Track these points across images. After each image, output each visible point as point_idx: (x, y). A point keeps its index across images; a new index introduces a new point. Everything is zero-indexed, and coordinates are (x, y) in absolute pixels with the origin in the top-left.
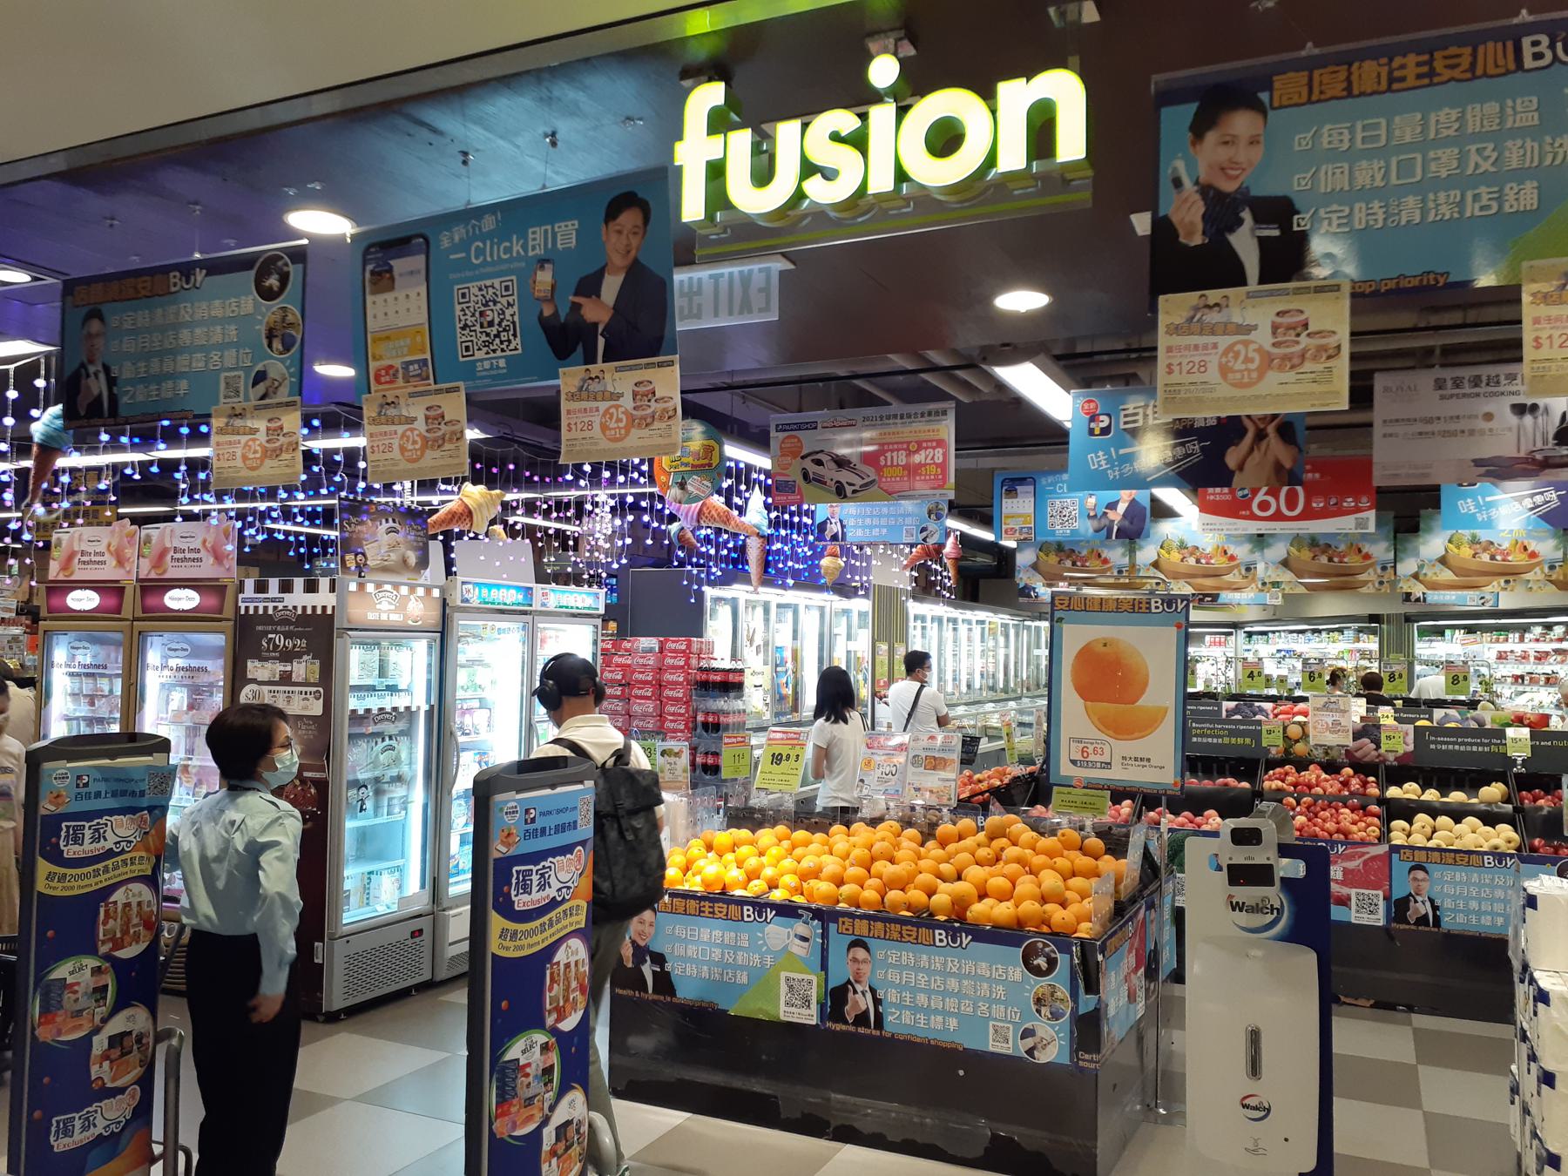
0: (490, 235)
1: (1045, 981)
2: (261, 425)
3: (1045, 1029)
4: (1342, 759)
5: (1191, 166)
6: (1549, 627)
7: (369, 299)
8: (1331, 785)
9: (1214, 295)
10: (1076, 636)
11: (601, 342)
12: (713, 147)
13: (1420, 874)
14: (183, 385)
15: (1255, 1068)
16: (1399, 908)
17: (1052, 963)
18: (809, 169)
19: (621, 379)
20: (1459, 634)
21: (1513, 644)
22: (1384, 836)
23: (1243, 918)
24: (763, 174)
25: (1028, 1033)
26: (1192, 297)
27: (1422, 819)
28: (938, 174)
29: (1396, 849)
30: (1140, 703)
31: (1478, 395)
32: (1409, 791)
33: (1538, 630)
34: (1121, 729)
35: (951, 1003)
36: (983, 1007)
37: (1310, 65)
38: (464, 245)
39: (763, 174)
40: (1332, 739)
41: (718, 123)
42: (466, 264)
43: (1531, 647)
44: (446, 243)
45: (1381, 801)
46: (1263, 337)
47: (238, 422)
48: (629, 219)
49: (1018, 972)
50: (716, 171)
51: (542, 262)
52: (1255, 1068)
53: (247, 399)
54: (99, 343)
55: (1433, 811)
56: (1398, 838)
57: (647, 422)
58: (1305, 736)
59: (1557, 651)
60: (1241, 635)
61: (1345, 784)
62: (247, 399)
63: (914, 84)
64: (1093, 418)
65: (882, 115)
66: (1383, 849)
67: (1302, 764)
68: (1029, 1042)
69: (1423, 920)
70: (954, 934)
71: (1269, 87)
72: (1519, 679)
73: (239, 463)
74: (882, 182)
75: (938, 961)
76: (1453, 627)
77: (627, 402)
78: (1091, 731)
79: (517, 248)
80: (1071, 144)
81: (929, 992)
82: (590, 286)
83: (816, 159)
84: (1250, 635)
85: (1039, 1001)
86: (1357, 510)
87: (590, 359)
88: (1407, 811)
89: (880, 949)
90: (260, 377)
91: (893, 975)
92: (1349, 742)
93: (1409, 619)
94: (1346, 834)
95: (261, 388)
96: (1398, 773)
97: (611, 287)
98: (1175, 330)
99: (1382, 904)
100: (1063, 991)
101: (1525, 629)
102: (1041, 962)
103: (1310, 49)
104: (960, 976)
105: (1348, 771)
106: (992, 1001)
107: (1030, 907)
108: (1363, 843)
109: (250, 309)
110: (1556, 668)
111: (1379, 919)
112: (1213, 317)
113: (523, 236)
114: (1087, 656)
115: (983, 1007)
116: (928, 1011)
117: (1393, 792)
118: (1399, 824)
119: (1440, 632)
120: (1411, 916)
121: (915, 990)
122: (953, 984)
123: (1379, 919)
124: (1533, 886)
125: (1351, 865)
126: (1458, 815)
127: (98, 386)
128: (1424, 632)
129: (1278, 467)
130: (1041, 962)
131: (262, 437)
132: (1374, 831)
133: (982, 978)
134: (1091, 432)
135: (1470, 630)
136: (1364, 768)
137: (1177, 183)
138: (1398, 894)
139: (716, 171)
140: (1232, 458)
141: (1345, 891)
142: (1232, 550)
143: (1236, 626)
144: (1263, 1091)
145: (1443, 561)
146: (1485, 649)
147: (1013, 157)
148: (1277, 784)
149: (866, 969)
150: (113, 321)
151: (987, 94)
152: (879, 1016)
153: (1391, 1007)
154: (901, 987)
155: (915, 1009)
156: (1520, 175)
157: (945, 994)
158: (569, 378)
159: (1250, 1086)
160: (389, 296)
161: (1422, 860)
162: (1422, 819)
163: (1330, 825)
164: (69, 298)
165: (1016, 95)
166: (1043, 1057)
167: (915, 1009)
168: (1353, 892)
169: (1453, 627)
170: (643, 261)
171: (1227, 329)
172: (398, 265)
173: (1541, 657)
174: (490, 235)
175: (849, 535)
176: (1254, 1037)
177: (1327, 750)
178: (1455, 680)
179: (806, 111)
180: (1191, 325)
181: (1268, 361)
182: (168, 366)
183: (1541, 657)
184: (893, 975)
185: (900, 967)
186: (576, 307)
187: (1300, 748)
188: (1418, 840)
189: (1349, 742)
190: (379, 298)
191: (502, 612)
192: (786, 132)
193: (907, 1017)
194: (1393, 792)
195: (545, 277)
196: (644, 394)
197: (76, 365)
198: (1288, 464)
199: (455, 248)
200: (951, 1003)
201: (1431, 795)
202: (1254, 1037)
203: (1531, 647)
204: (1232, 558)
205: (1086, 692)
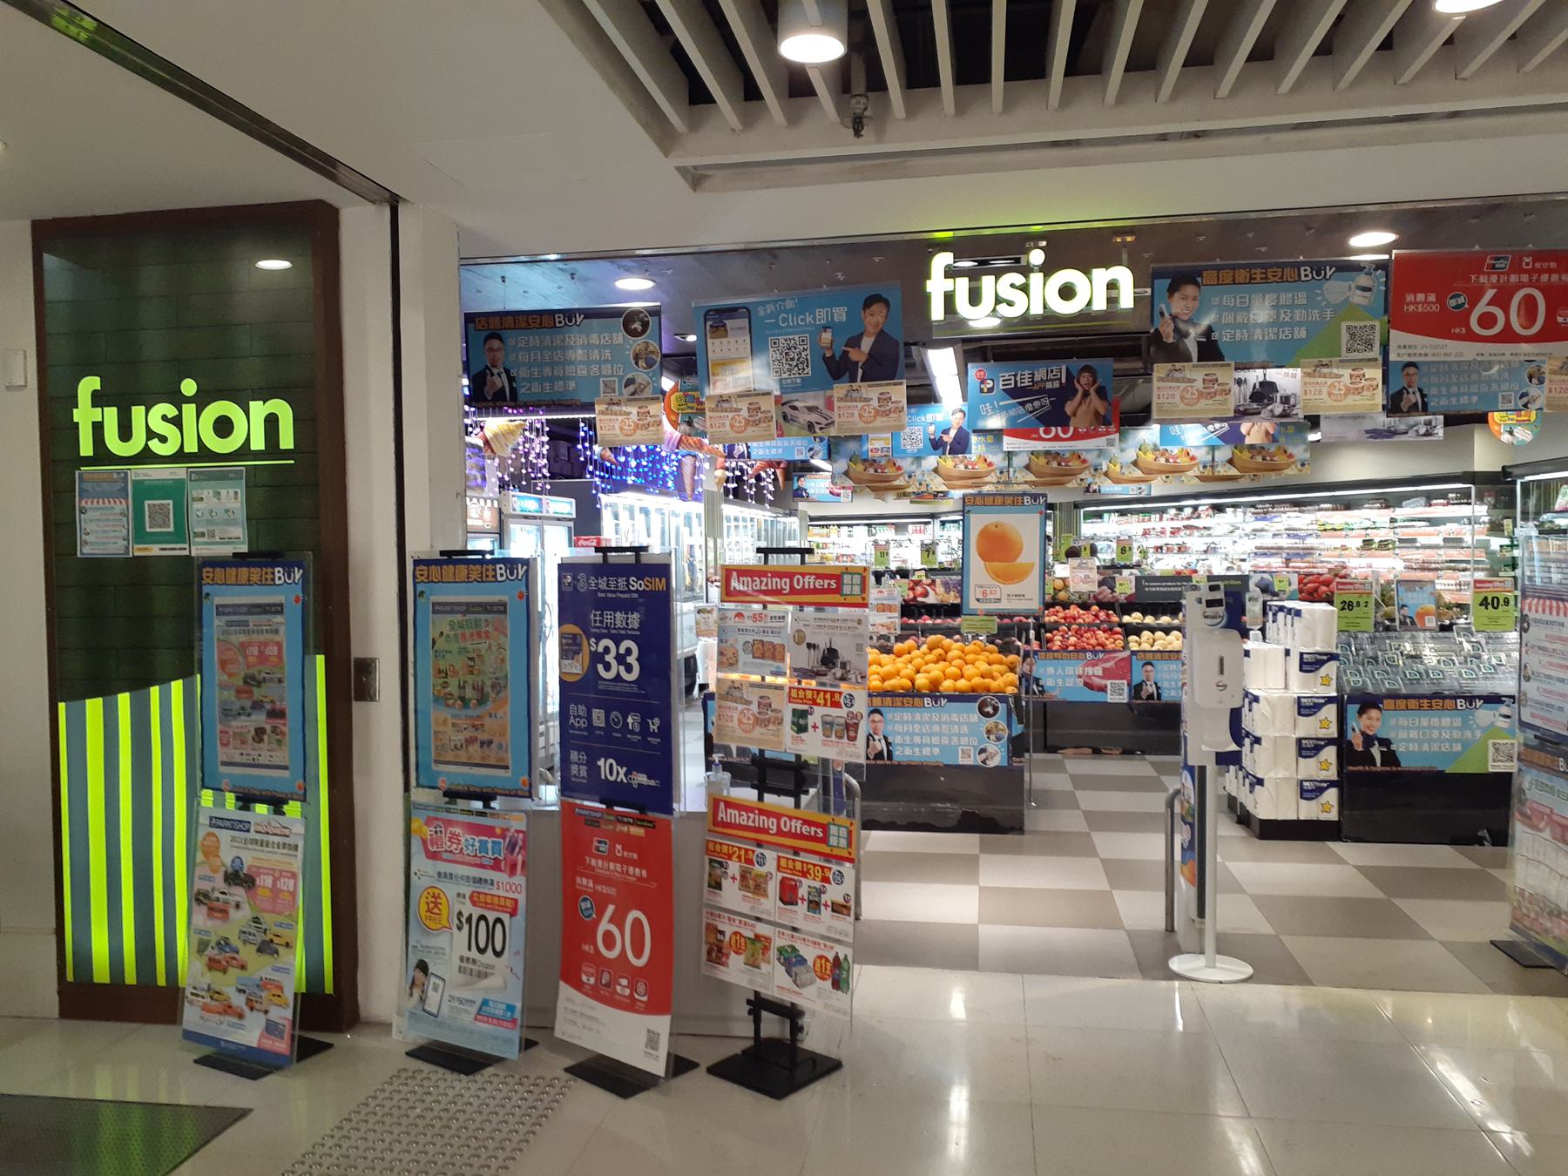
0: (792, 311)
1: (992, 720)
2: (633, 410)
3: (992, 747)
4: (1092, 600)
5: (1168, 307)
6: (1180, 509)
7: (710, 341)
8: (1087, 617)
9: (1178, 365)
10: (979, 521)
11: (860, 372)
13: (1149, 668)
14: (572, 385)
15: (1222, 672)
16: (1136, 690)
17: (996, 709)
19: (872, 391)
20: (1114, 517)
21: (1154, 522)
22: (1125, 647)
23: (1209, 621)
25: (983, 751)
26: (1169, 366)
27: (1146, 634)
29: (1134, 653)
30: (1019, 560)
32: (1135, 618)
33: (1173, 512)
34: (1006, 577)
35: (935, 740)
36: (955, 739)
37: (1218, 268)
38: (775, 315)
40: (1085, 588)
42: (776, 325)
43: (1168, 524)
45: (1121, 625)
46: (1199, 385)
47: (615, 408)
49: (975, 716)
51: (825, 328)
52: (1222, 672)
53: (621, 394)
54: (499, 355)
55: (1153, 630)
56: (1134, 647)
57: (887, 413)
58: (1066, 587)
59: (1186, 527)
60: (937, 523)
61: (1096, 616)
62: (621, 394)
64: (983, 382)
65: (1036, 279)
66: (1127, 653)
67: (1066, 605)
68: (984, 756)
69: (1150, 697)
70: (936, 699)
71: (1200, 275)
72: (1159, 549)
73: (618, 432)
74: (1037, 310)
75: (926, 716)
76: (1109, 512)
77: (875, 403)
78: (987, 580)
79: (809, 319)
81: (921, 735)
82: (855, 342)
84: (943, 523)
85: (989, 732)
86: (1108, 433)
87: (853, 379)
88: (1136, 630)
89: (890, 714)
91: (898, 728)
92: (1096, 589)
93: (1077, 506)
94: (1103, 646)
95: (631, 388)
96: (1127, 608)
97: (867, 343)
98: (1161, 379)
99: (1126, 688)
100: (1003, 725)
101: (1163, 511)
102: (990, 709)
103: (1218, 262)
104: (940, 723)
105: (1095, 608)
106: (959, 735)
107: (977, 680)
108: (1115, 651)
109: (620, 340)
110: (1186, 540)
111: (1124, 699)
112: (1177, 375)
113: (812, 313)
114: (985, 534)
115: (955, 739)
116: (921, 746)
117: (1126, 619)
118: (1133, 638)
119: (1099, 515)
120: (1144, 695)
121: (912, 735)
122: (936, 728)
123: (1124, 699)
124: (1246, 647)
125: (1107, 665)
126: (1167, 630)
127: (501, 381)
128: (1088, 516)
129: (1097, 413)
130: (990, 709)
131: (634, 417)
132: (1120, 643)
133: (954, 723)
134: (982, 391)
135: (1122, 513)
136: (1104, 606)
137: (1162, 314)
138: (1135, 681)
140: (1069, 408)
141: (1103, 682)
142: (990, 458)
143: (933, 516)
144: (1224, 679)
145: (1135, 463)
146: (1132, 527)
148: (1053, 618)
149: (881, 726)
150: (511, 342)
151: (1087, 272)
152: (889, 752)
153: (1133, 753)
154: (903, 734)
155: (912, 746)
156: (1300, 324)
157: (931, 735)
158: (840, 389)
159: (1220, 678)
160: (724, 340)
161: (1150, 658)
162: (1146, 634)
163: (1093, 641)
164: (471, 326)
165: (1101, 276)
166: (992, 764)
167: (912, 746)
168: (1108, 682)
169: (1109, 512)
171: (1184, 380)
172: (729, 323)
173: (1174, 532)
175: (753, 454)
176: (1221, 660)
177: (1081, 594)
178: (1123, 550)
180: (846, 398)
181: (1201, 394)
182: (558, 372)
183: (1174, 532)
184: (898, 728)
185: (902, 722)
186: (845, 353)
187: (1062, 595)
188: (1146, 646)
189: (1096, 589)
191: (526, 517)
193: (908, 752)
194: (1126, 619)
195: (827, 337)
196: (884, 399)
197: (481, 367)
198: (1102, 412)
200: (935, 740)
201: (1149, 620)
202: (1221, 660)
203: (1168, 524)
204: (990, 464)
205: (985, 556)
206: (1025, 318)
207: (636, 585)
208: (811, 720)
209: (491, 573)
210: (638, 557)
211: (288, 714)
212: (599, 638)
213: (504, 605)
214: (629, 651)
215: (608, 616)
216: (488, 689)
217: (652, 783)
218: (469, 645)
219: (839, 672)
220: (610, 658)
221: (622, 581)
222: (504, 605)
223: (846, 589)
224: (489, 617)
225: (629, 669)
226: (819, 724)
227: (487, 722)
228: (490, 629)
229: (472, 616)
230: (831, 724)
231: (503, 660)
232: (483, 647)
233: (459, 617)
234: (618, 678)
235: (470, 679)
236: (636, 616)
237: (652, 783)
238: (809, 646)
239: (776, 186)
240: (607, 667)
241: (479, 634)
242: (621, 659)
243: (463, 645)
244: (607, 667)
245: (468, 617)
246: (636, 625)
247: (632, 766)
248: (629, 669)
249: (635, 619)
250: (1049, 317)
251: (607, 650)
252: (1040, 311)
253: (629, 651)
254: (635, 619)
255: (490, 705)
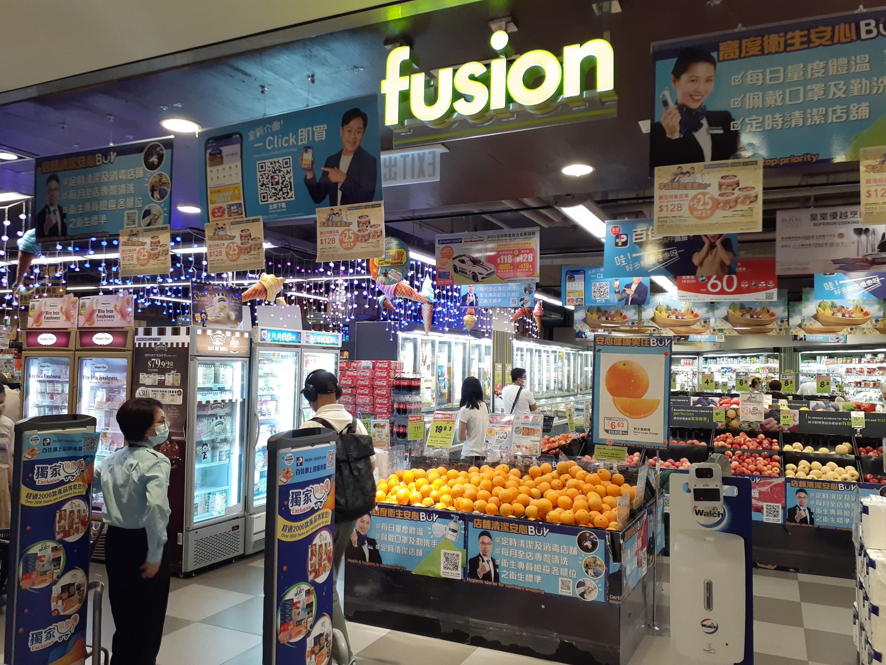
0: (277, 133)
1: (591, 555)
2: (148, 240)
3: (590, 582)
4: (758, 429)
5: (673, 94)
6: (875, 355)
7: (209, 169)
8: (752, 444)
9: (686, 167)
10: (608, 360)
11: (340, 193)
12: (403, 83)
13: (802, 494)
14: (104, 218)
15: (709, 604)
16: (790, 514)
17: (594, 544)
18: (457, 95)
19: (351, 214)
20: (824, 359)
21: (855, 364)
22: (782, 473)
23: (702, 519)
24: (431, 98)
25: (581, 584)
26: (674, 168)
27: (803, 463)
28: (530, 98)
29: (789, 480)
30: (644, 397)
31: (835, 223)
32: (796, 447)
33: (869, 356)
34: (634, 412)
35: (537, 567)
36: (556, 569)
37: (740, 37)
38: (262, 139)
39: (431, 98)
40: (752, 418)
41: (406, 70)
42: (263, 149)
43: (865, 366)
44: (252, 138)
45: (781, 453)
46: (714, 191)
47: (134, 239)
48: (355, 124)
49: (575, 550)
50: (405, 97)
51: (306, 148)
52: (709, 604)
53: (140, 226)
54: (56, 194)
55: (810, 459)
56: (790, 474)
57: (366, 239)
58: (737, 416)
59: (880, 368)
60: (701, 359)
61: (760, 443)
62: (140, 226)
63: (517, 48)
64: (618, 236)
65: (498, 65)
66: (781, 480)
67: (736, 432)
68: (582, 589)
69: (804, 520)
70: (539, 528)
71: (717, 49)
72: (858, 384)
73: (135, 262)
74: (498, 103)
75: (530, 544)
76: (821, 355)
77: (354, 228)
78: (616, 414)
79: (292, 140)
80: (605, 81)
81: (525, 561)
82: (333, 162)
83: (461, 90)
84: (706, 359)
85: (587, 566)
86: (767, 288)
87: (333, 203)
88: (795, 459)
89: (497, 537)
90: (147, 213)
91: (505, 552)
92: (762, 420)
93: (796, 350)
94: (761, 471)
95: (148, 219)
96: (790, 437)
97: (345, 162)
98: (664, 186)
99: (781, 511)
100: (601, 561)
101: (861, 356)
102: (588, 544)
103: (740, 28)
104: (542, 552)
105: (762, 436)
106: (560, 566)
107: (582, 513)
108: (770, 477)
109: (141, 175)
110: (879, 378)
111: (779, 520)
112: (685, 179)
113: (296, 133)
114: (614, 371)
115: (556, 569)
116: (524, 572)
117: (787, 448)
118: (790, 466)
119: (814, 357)
120: (798, 518)
121: (517, 560)
122: (538, 556)
123: (779, 520)
124: (866, 501)
125: (763, 489)
126: (824, 461)
127: (55, 218)
128: (805, 357)
129: (722, 264)
130: (588, 544)
131: (148, 247)
132: (777, 470)
133: (555, 553)
134: (617, 244)
135: (831, 356)
136: (771, 434)
137: (665, 103)
138: (790, 505)
139: (405, 97)
140: (696, 259)
141: (760, 504)
142: (696, 311)
143: (698, 354)
144: (714, 617)
145: (815, 317)
146: (839, 367)
147: (572, 89)
148: (722, 443)
149: (489, 548)
150: (64, 182)
151: (558, 53)
152: (497, 575)
153: (786, 569)
154: (509, 558)
155: (517, 571)
156: (859, 99)
157: (534, 562)
158: (321, 214)
159: (706, 614)
160: (220, 167)
161: (803, 486)
162: (803, 463)
163: (752, 467)
164: (39, 169)
165: (574, 54)
166: (589, 598)
167: (517, 571)
168: (765, 504)
169: (821, 355)
170: (363, 147)
171: (693, 186)
172: (225, 150)
173: (871, 372)
174: (277, 133)
175: (480, 303)
176: (709, 586)
177: (750, 424)
178: (822, 385)
179: (455, 63)
180: (673, 184)
181: (716, 204)
182: (95, 207)
183: (871, 372)
184: (505, 552)
185: (508, 547)
186: (326, 174)
187: (734, 423)
188: (801, 475)
189: (762, 420)
190: (214, 169)
191: (284, 346)
192: (444, 75)
193: (512, 575)
194: (787, 448)
195: (308, 157)
196: (364, 223)
197: (43, 206)
198: (728, 263)
199: (257, 140)
200: (537, 567)
201: (809, 450)
202: (709, 586)
203: (865, 366)
204: (696, 316)
205: (614, 391)
211: (880, 612)
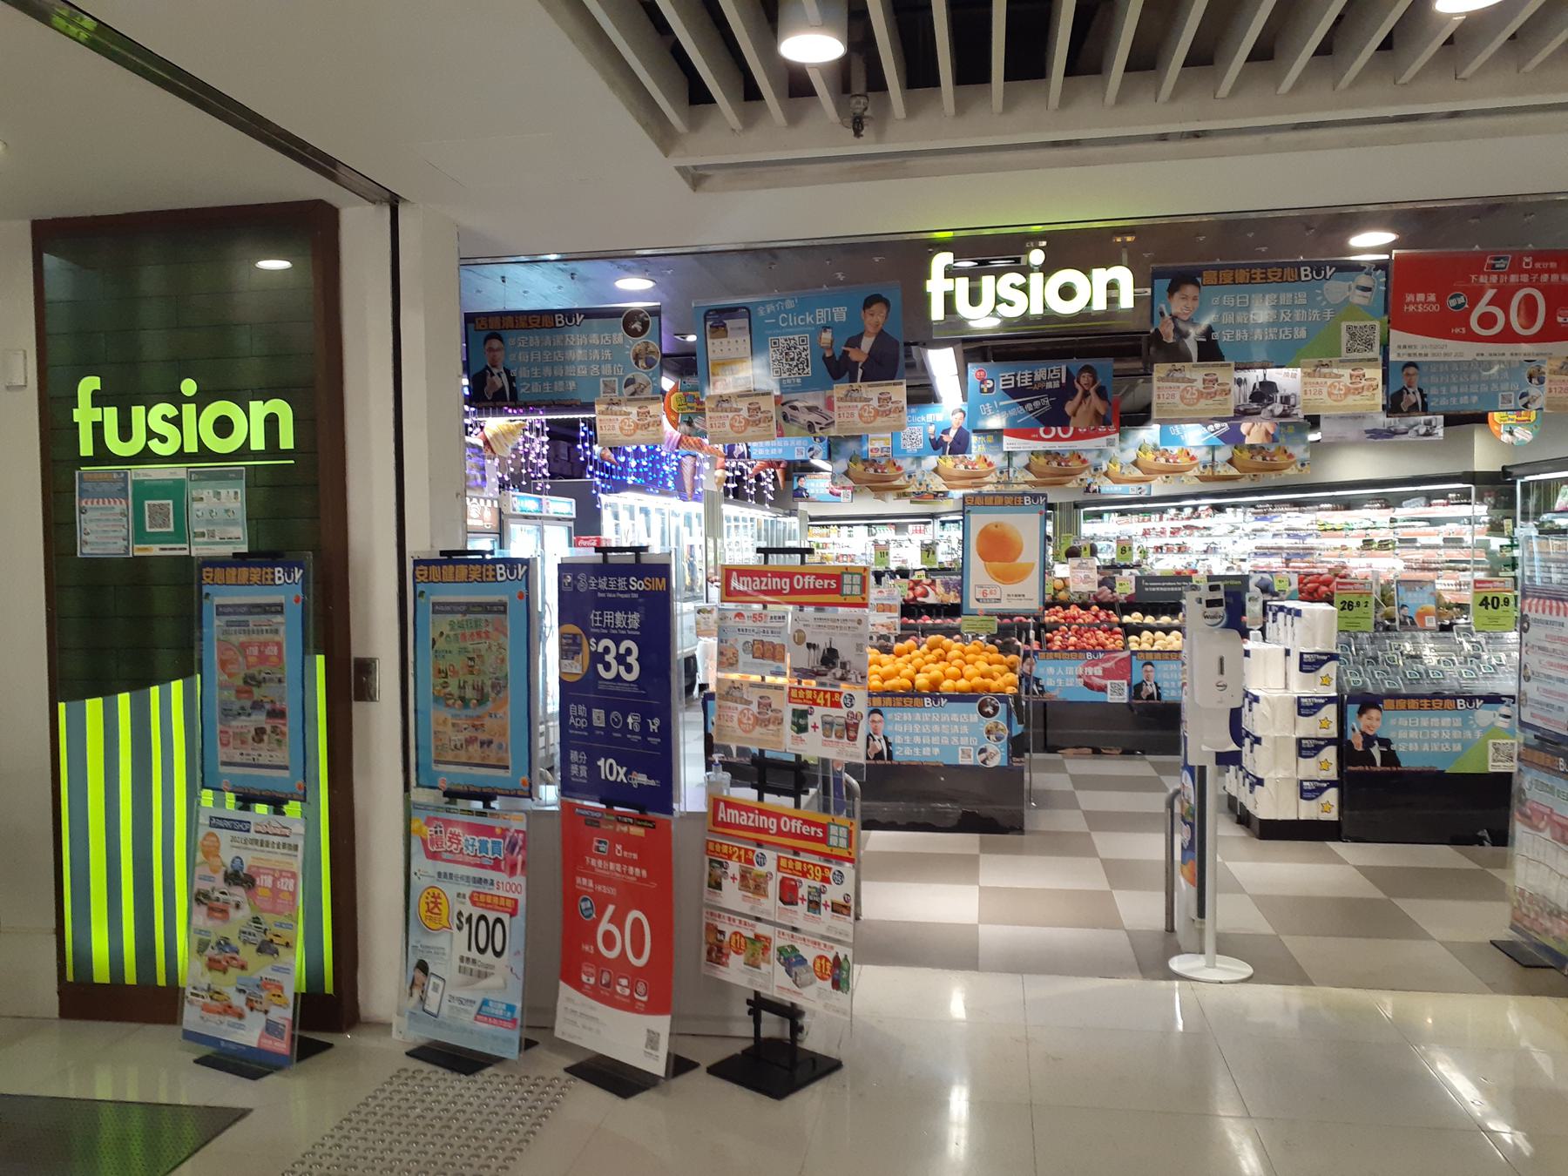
0: (792, 311)
1: (992, 720)
2: (633, 410)
3: (992, 747)
4: (1092, 600)
5: (1168, 307)
6: (1180, 509)
7: (710, 341)
8: (1087, 617)
9: (1178, 365)
10: (979, 521)
11: (860, 372)
13: (1149, 668)
14: (572, 385)
15: (1222, 672)
16: (1136, 690)
17: (996, 709)
19: (872, 391)
20: (1114, 517)
21: (1154, 522)
22: (1125, 647)
23: (1209, 621)
25: (983, 751)
26: (1169, 366)
27: (1146, 634)
29: (1134, 653)
30: (1019, 560)
32: (1135, 618)
33: (1173, 512)
34: (1006, 577)
35: (935, 740)
36: (955, 739)
37: (1218, 268)
38: (775, 315)
40: (1085, 588)
42: (776, 325)
43: (1168, 524)
45: (1121, 625)
46: (1199, 385)
47: (615, 408)
49: (975, 716)
51: (825, 328)
52: (1222, 672)
53: (621, 394)
54: (499, 355)
55: (1153, 630)
56: (1134, 647)
57: (887, 413)
58: (1066, 587)
59: (1186, 527)
60: (937, 523)
61: (1096, 616)
62: (621, 394)
64: (983, 382)
65: (1036, 279)
66: (1127, 653)
67: (1066, 605)
68: (984, 756)
69: (1150, 697)
70: (936, 699)
71: (1200, 275)
72: (1159, 549)
73: (618, 432)
74: (1037, 310)
75: (926, 716)
76: (1109, 512)
77: (875, 403)
78: (987, 580)
79: (809, 319)
81: (921, 735)
82: (855, 342)
84: (943, 523)
85: (989, 732)
86: (1108, 433)
87: (853, 379)
88: (1136, 630)
89: (890, 714)
91: (898, 728)
92: (1096, 589)
93: (1077, 506)
94: (1103, 646)
95: (631, 388)
96: (1127, 608)
97: (867, 343)
98: (1161, 379)
99: (1126, 688)
100: (1003, 725)
101: (1163, 511)
102: (990, 709)
103: (1218, 262)
104: (940, 723)
105: (1095, 608)
106: (959, 735)
107: (977, 680)
108: (1115, 651)
109: (620, 340)
110: (1186, 540)
111: (1124, 699)
112: (1177, 375)
113: (812, 313)
114: (985, 534)
115: (955, 739)
116: (921, 746)
117: (1126, 619)
118: (1133, 638)
119: (1099, 515)
120: (1144, 695)
121: (912, 735)
122: (936, 728)
123: (1124, 699)
124: (1246, 647)
125: (1107, 665)
126: (1167, 630)
127: (501, 381)
128: (1088, 516)
129: (1097, 413)
130: (990, 709)
131: (634, 417)
132: (1120, 643)
133: (954, 723)
134: (982, 391)
135: (1122, 513)
136: (1104, 606)
137: (1162, 314)
138: (1135, 681)
140: (1069, 408)
141: (1103, 682)
142: (990, 458)
143: (933, 516)
144: (1224, 679)
145: (1135, 463)
146: (1132, 527)
148: (1053, 618)
149: (881, 726)
150: (511, 342)
151: (1087, 272)
152: (889, 752)
153: (1133, 753)
154: (903, 734)
155: (912, 746)
156: (1300, 324)
157: (931, 735)
158: (840, 389)
159: (1220, 678)
160: (724, 340)
161: (1150, 658)
162: (1146, 634)
163: (1093, 641)
164: (471, 326)
165: (1101, 276)
166: (992, 764)
167: (912, 746)
168: (1108, 682)
169: (1109, 512)
171: (1184, 380)
172: (729, 323)
173: (1174, 532)
175: (753, 454)
176: (1221, 660)
177: (1081, 594)
178: (1123, 550)
180: (846, 398)
181: (1201, 394)
182: (558, 372)
183: (1174, 532)
184: (898, 728)
185: (902, 722)
186: (845, 353)
187: (1062, 595)
188: (1146, 646)
189: (1096, 589)
191: (526, 517)
193: (908, 752)
194: (1126, 619)
195: (827, 337)
196: (884, 399)
197: (481, 367)
198: (1102, 412)
200: (935, 740)
201: (1149, 620)
202: (1221, 660)
203: (1168, 524)
204: (990, 464)
205: (985, 556)
206: (1025, 318)
207: (636, 585)
208: (811, 720)
209: (491, 573)
210: (638, 557)
212: (599, 638)
213: (504, 605)
214: (629, 651)
215: (608, 616)
216: (488, 689)
217: (652, 783)
218: (469, 645)
219: (839, 672)
220: (610, 658)
221: (622, 581)
222: (504, 605)
223: (846, 589)
224: (489, 617)
225: (629, 669)
226: (819, 724)
227: (487, 722)
228: (490, 629)
229: (472, 616)
230: (831, 724)
231: (503, 660)
232: (483, 647)
233: (459, 617)
234: (618, 678)
235: (470, 679)
236: (636, 616)
237: (652, 783)
238: (809, 646)
239: (776, 186)
240: (607, 667)
241: (479, 634)
242: (621, 659)
243: (463, 645)
244: (607, 667)
245: (468, 617)
246: (636, 625)
247: (632, 766)
248: (629, 669)
249: (635, 619)
250: (1049, 317)
251: (607, 650)
252: (1040, 311)
253: (629, 651)
254: (635, 619)
255: (490, 705)
